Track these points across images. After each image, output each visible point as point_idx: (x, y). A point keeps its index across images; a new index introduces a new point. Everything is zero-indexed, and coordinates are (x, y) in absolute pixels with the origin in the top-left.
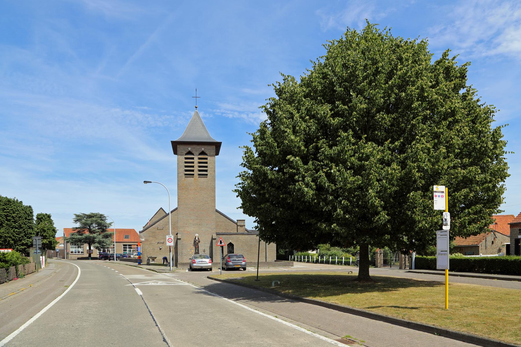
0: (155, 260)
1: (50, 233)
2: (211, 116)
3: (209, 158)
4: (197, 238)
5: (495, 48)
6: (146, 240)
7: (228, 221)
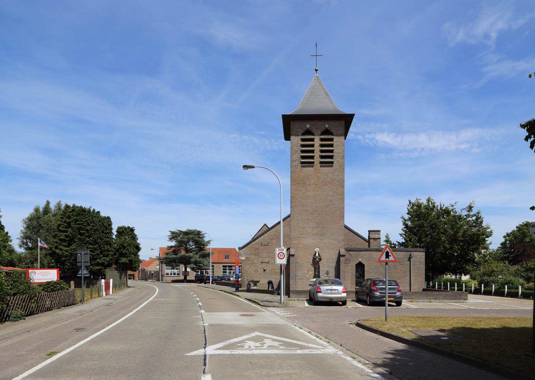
0: (258, 284)
1: (132, 250)
3: (336, 138)
4: (317, 255)
6: (247, 259)
7: (352, 234)
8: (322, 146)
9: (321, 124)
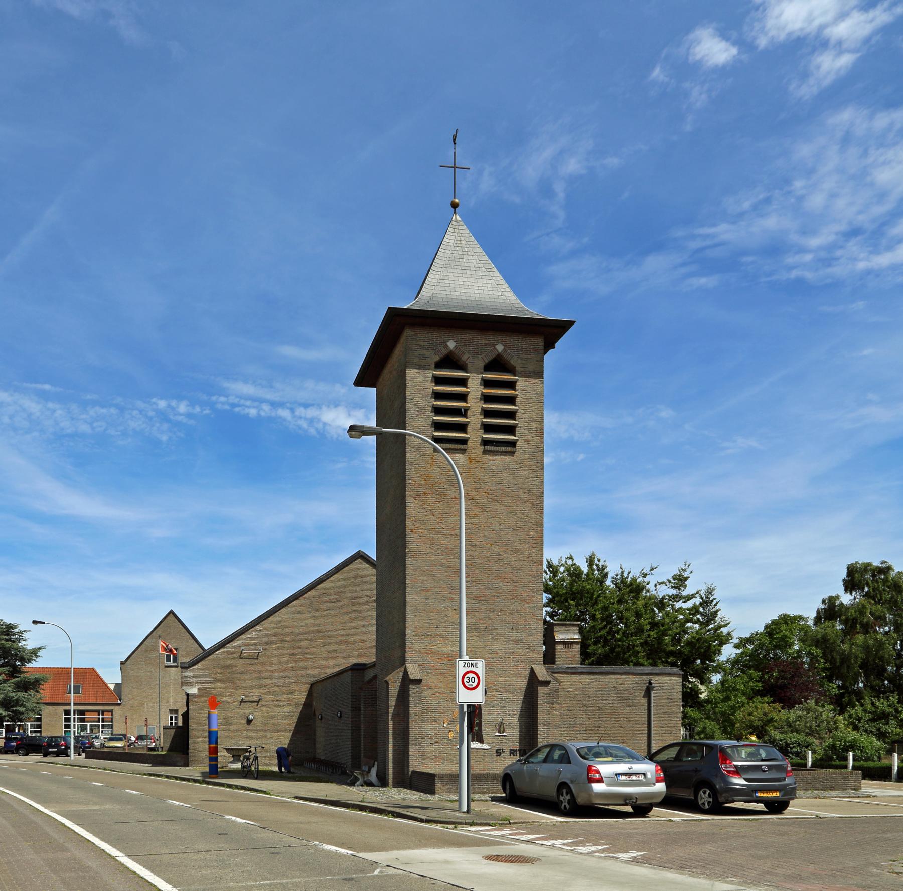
2: (207, 412)
3: (522, 383)
5: (890, 248)
8: (487, 398)
9: (483, 342)
